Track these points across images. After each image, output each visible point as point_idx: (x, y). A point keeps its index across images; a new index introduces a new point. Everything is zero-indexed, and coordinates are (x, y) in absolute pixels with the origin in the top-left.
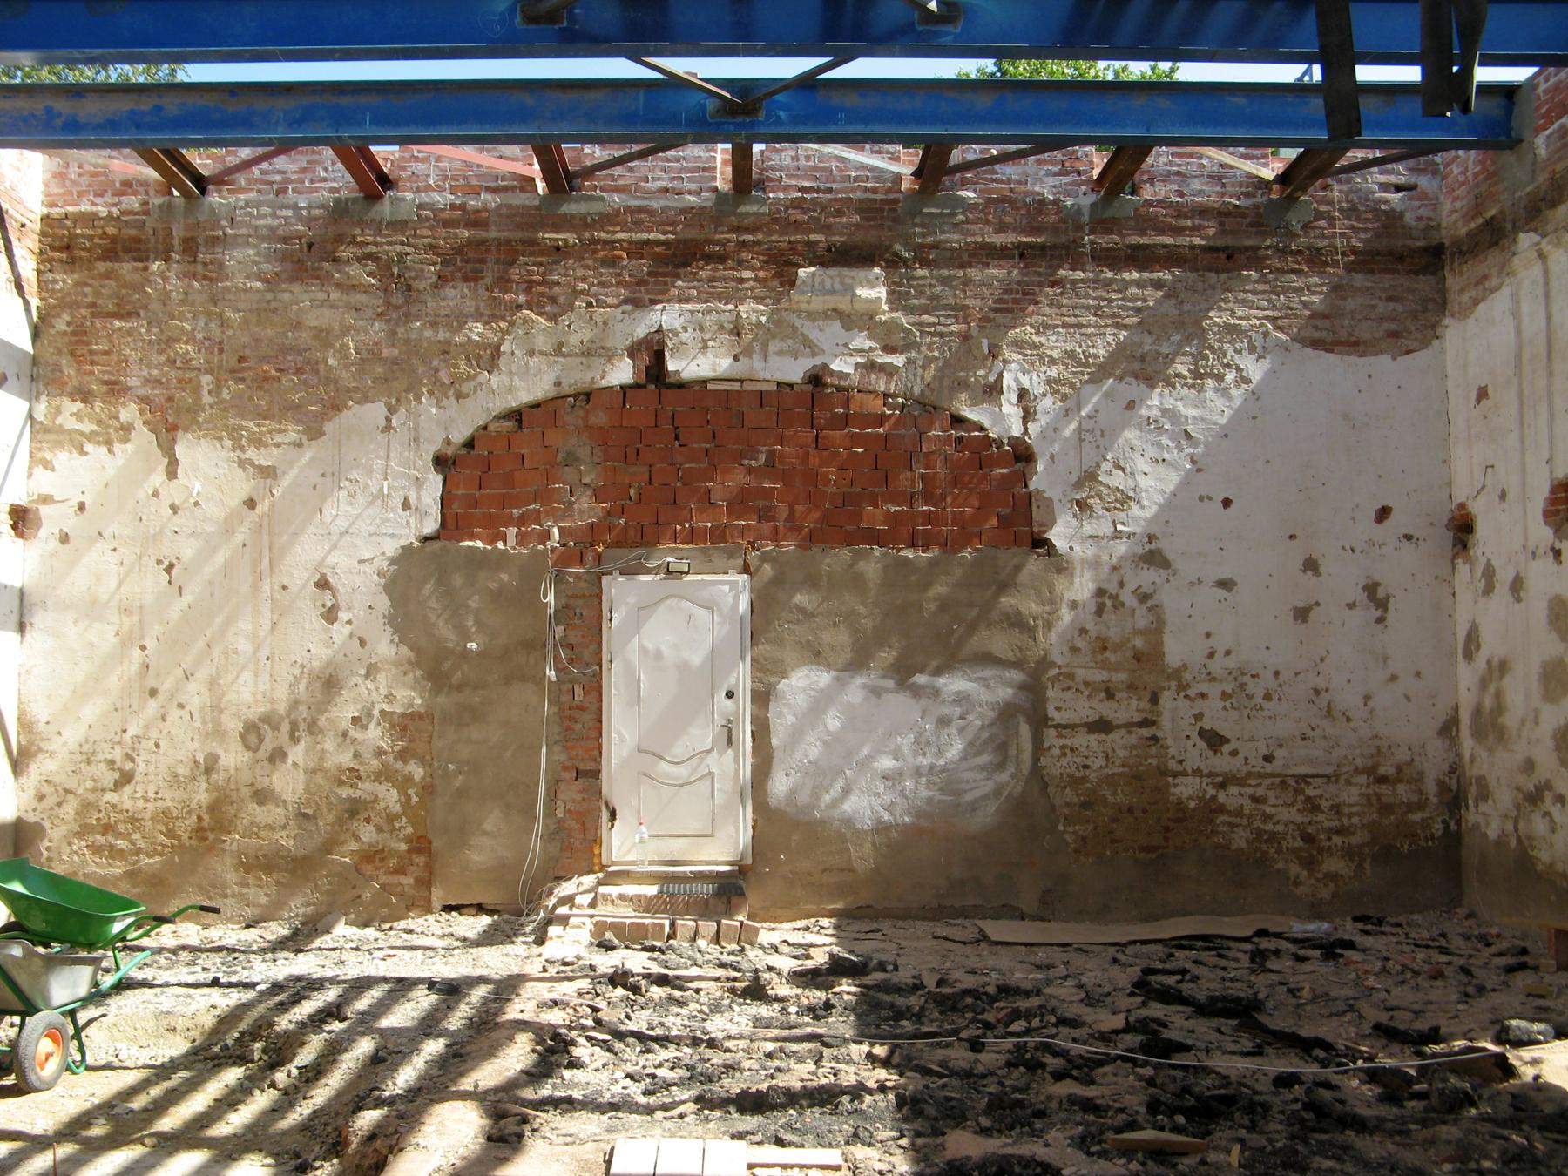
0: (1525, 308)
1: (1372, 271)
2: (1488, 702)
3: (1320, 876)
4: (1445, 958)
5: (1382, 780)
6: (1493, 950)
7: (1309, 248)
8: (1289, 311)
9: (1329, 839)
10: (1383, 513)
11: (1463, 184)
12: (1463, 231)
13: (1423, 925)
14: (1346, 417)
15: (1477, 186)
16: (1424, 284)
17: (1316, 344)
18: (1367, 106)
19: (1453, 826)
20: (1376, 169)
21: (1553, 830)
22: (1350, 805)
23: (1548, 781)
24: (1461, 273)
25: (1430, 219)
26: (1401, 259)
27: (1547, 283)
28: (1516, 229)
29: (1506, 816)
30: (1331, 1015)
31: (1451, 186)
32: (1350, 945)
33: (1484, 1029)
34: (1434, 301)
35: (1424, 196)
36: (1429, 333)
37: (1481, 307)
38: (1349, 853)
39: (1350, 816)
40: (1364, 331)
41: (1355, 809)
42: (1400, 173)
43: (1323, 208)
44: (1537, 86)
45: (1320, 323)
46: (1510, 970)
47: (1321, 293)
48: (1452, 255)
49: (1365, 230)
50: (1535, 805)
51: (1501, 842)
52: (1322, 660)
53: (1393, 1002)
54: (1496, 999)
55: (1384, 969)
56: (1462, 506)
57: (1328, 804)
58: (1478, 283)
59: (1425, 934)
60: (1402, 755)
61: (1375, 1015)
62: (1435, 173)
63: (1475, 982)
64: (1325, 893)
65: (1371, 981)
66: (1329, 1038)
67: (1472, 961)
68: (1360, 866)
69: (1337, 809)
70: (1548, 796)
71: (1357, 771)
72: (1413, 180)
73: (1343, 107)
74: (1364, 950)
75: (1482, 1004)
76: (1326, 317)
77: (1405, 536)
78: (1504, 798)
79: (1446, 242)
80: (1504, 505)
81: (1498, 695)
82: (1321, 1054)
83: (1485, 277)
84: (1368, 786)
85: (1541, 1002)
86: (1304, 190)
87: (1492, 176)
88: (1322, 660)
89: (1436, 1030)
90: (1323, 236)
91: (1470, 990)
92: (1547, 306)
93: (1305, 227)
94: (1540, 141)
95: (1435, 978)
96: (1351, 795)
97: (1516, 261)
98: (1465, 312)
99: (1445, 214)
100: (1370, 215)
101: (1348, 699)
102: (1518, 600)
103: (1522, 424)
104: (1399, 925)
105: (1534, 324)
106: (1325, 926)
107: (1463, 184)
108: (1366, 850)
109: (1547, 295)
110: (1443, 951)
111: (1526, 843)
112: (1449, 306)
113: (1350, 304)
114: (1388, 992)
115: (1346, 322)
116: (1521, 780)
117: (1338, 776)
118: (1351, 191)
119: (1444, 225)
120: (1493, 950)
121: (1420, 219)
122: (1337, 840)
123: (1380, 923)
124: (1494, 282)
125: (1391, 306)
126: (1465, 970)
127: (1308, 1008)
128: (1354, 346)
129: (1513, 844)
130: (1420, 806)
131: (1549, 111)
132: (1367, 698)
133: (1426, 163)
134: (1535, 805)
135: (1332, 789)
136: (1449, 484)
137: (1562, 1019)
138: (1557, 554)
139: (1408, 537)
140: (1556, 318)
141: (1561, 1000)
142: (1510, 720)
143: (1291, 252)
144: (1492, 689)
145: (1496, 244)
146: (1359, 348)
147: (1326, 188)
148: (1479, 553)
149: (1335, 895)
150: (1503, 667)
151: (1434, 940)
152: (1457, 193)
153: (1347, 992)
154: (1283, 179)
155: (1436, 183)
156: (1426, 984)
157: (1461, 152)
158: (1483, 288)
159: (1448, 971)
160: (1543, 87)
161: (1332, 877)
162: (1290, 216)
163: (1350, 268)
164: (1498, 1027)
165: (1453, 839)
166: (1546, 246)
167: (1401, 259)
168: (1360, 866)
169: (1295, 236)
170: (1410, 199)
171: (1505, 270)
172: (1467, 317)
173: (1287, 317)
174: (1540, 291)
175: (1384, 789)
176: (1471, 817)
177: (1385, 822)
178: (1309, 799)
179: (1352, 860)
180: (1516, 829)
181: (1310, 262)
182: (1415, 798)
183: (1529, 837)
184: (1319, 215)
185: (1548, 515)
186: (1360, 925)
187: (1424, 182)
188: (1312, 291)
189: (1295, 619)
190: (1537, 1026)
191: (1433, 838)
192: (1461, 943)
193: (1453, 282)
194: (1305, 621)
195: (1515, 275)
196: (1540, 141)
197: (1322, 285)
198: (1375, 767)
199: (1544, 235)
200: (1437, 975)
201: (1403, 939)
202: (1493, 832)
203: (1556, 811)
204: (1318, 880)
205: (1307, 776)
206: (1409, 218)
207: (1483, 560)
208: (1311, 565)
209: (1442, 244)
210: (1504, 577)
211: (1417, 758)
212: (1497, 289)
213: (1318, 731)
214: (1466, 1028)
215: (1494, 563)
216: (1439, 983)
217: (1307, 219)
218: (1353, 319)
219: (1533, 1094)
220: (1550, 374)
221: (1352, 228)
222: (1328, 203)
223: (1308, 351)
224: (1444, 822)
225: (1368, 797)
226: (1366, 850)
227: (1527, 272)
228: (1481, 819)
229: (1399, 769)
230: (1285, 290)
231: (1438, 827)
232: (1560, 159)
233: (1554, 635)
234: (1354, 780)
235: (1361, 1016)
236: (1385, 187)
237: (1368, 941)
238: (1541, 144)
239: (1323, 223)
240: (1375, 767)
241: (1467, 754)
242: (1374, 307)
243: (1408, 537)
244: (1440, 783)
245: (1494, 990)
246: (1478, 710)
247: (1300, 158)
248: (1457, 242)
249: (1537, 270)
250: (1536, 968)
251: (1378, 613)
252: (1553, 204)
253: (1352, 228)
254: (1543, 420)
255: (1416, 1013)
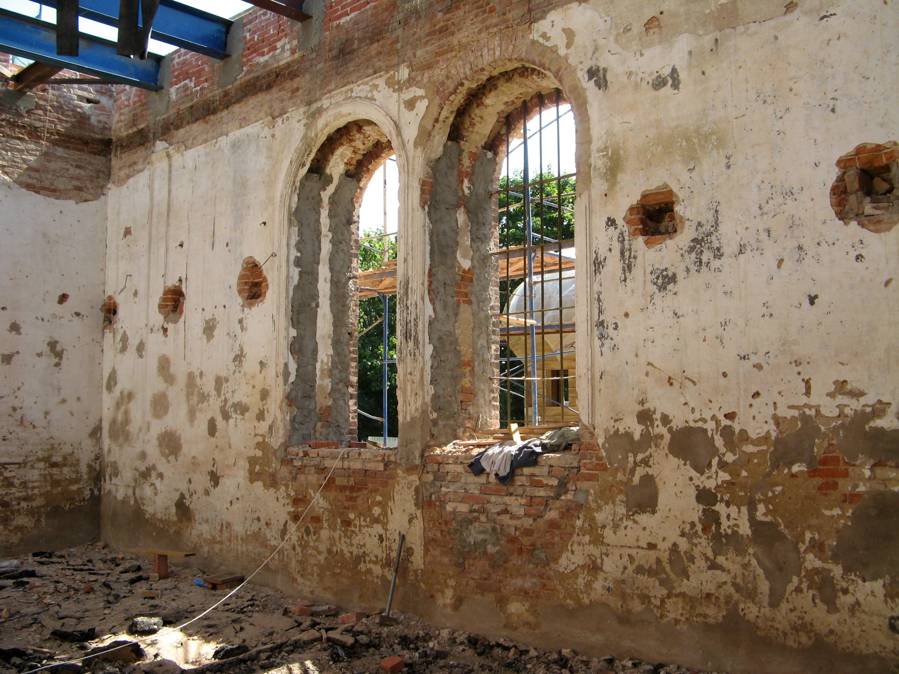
0: (156, 185)
1: (68, 148)
2: (120, 417)
3: (11, 528)
4: (93, 578)
5: (55, 465)
6: (120, 568)
7: (30, 126)
8: (13, 164)
9: (19, 504)
10: (63, 298)
11: (126, 106)
12: (124, 134)
13: (78, 555)
14: (44, 235)
15: (135, 109)
16: (98, 161)
17: (29, 187)
18: (82, 44)
19: (96, 493)
20: (76, 86)
21: (156, 494)
22: (33, 482)
23: (154, 465)
24: (121, 158)
25: (106, 123)
26: (86, 143)
27: (170, 172)
28: (155, 138)
29: (128, 486)
30: (23, 627)
31: (119, 107)
32: (32, 574)
33: (121, 625)
34: (103, 172)
35: (103, 109)
36: (99, 191)
37: (131, 180)
38: (31, 512)
39: (33, 488)
40: (60, 184)
41: (36, 484)
42: (90, 91)
43: (41, 102)
44: (174, 59)
45: (33, 174)
46: (133, 582)
47: (35, 155)
48: (117, 147)
49: (67, 122)
50: (146, 479)
51: (124, 501)
52: (19, 389)
53: (63, 613)
54: (127, 603)
55: (56, 590)
56: (110, 298)
57: (19, 482)
58: (130, 166)
59: (79, 561)
60: (67, 449)
61: (54, 624)
62: (111, 96)
63: (113, 592)
64: (15, 539)
65: (48, 600)
66: (21, 646)
67: (110, 578)
68: (38, 520)
69: (24, 484)
70: (154, 474)
71: (39, 460)
72: (98, 98)
73: (68, 38)
74: (41, 577)
75: (118, 607)
76: (37, 170)
77: (76, 313)
78: (127, 475)
79: (114, 139)
80: (136, 299)
81: (126, 413)
82: (16, 660)
83: (135, 163)
84: (45, 469)
85: (152, 602)
86: (31, 88)
87: (144, 105)
88: (19, 389)
89: (92, 630)
90: (40, 120)
91: (111, 598)
92: (169, 185)
93: (29, 112)
94: (173, 90)
95: (89, 593)
96: (33, 475)
97: (154, 157)
98: (121, 182)
99: (114, 122)
100: (70, 113)
101: (34, 414)
102: (141, 356)
103: (150, 252)
104: (62, 557)
105: (161, 195)
106: (15, 562)
107: (126, 106)
108: (43, 510)
109: (170, 179)
110: (91, 572)
111: (140, 501)
112: (112, 177)
113: (52, 166)
114: (59, 606)
115: (50, 176)
116: (138, 464)
117: (25, 463)
118: (60, 96)
119: (113, 128)
120: (120, 568)
121: (100, 122)
122: (24, 504)
123: (50, 555)
124: (140, 167)
125: (78, 171)
126: (106, 585)
127: (6, 624)
128: (53, 192)
129: (132, 502)
130: (77, 481)
131: (178, 75)
132: (47, 413)
133: (106, 89)
134: (146, 479)
135: (22, 471)
136: (104, 284)
137: (165, 612)
138: (165, 330)
139: (78, 314)
140: (174, 192)
141: (164, 599)
142: (133, 428)
143: (18, 126)
144: (123, 409)
145: (143, 144)
146: (57, 194)
147: (44, 90)
148: (119, 326)
149: (21, 540)
150: (130, 396)
151: (85, 565)
152: (123, 111)
153: (33, 609)
154: (18, 78)
155: (111, 102)
156: (83, 597)
157: (127, 87)
158: (133, 169)
159: (96, 586)
160: (177, 60)
161: (19, 528)
162: (19, 103)
163: (55, 143)
164: (130, 623)
165: (96, 500)
166: (171, 150)
167: (86, 143)
168: (38, 520)
169: (21, 116)
170: (95, 109)
171: (147, 161)
172: (122, 185)
173: (12, 166)
174: (166, 176)
175: (55, 471)
176: (107, 486)
177: (55, 491)
178: (6, 478)
179: (33, 517)
180: (134, 493)
181: (30, 134)
182: (74, 476)
183: (142, 499)
184: (38, 107)
185: (161, 307)
186: (38, 559)
187: (104, 100)
188: (30, 153)
189: (3, 362)
190: (155, 620)
191: (84, 500)
192: (100, 565)
193: (115, 163)
194: (9, 363)
195: (153, 165)
196: (173, 90)
197: (37, 150)
198: (50, 457)
199: (171, 144)
200: (90, 591)
201: (65, 566)
202: (120, 496)
203: (158, 483)
204: (10, 531)
205: (6, 464)
206: (93, 120)
207: (121, 331)
208: (15, 328)
209: (111, 140)
210: (134, 342)
211: (75, 451)
212: (141, 171)
213: (14, 434)
214: (111, 625)
215: (128, 333)
216: (92, 596)
217: (30, 107)
218: (54, 175)
219: (157, 669)
220: (168, 225)
221: (59, 119)
222: (46, 100)
223: (24, 190)
224: (91, 490)
225: (45, 476)
226: (43, 510)
227: (159, 164)
228: (113, 488)
229: (65, 458)
230: (12, 149)
231: (87, 493)
232: (183, 103)
233: (161, 378)
234: (36, 466)
235: (43, 626)
236: (81, 98)
237: (42, 570)
238: (173, 92)
239: (40, 112)
240: (50, 457)
241: (106, 449)
242: (68, 170)
243: (78, 314)
244: (90, 466)
245: (125, 597)
246: (114, 422)
247: (30, 67)
248: (120, 139)
249: (165, 164)
250: (147, 579)
251: (56, 360)
252: (177, 128)
253: (59, 119)
254: (162, 251)
255: (78, 619)
